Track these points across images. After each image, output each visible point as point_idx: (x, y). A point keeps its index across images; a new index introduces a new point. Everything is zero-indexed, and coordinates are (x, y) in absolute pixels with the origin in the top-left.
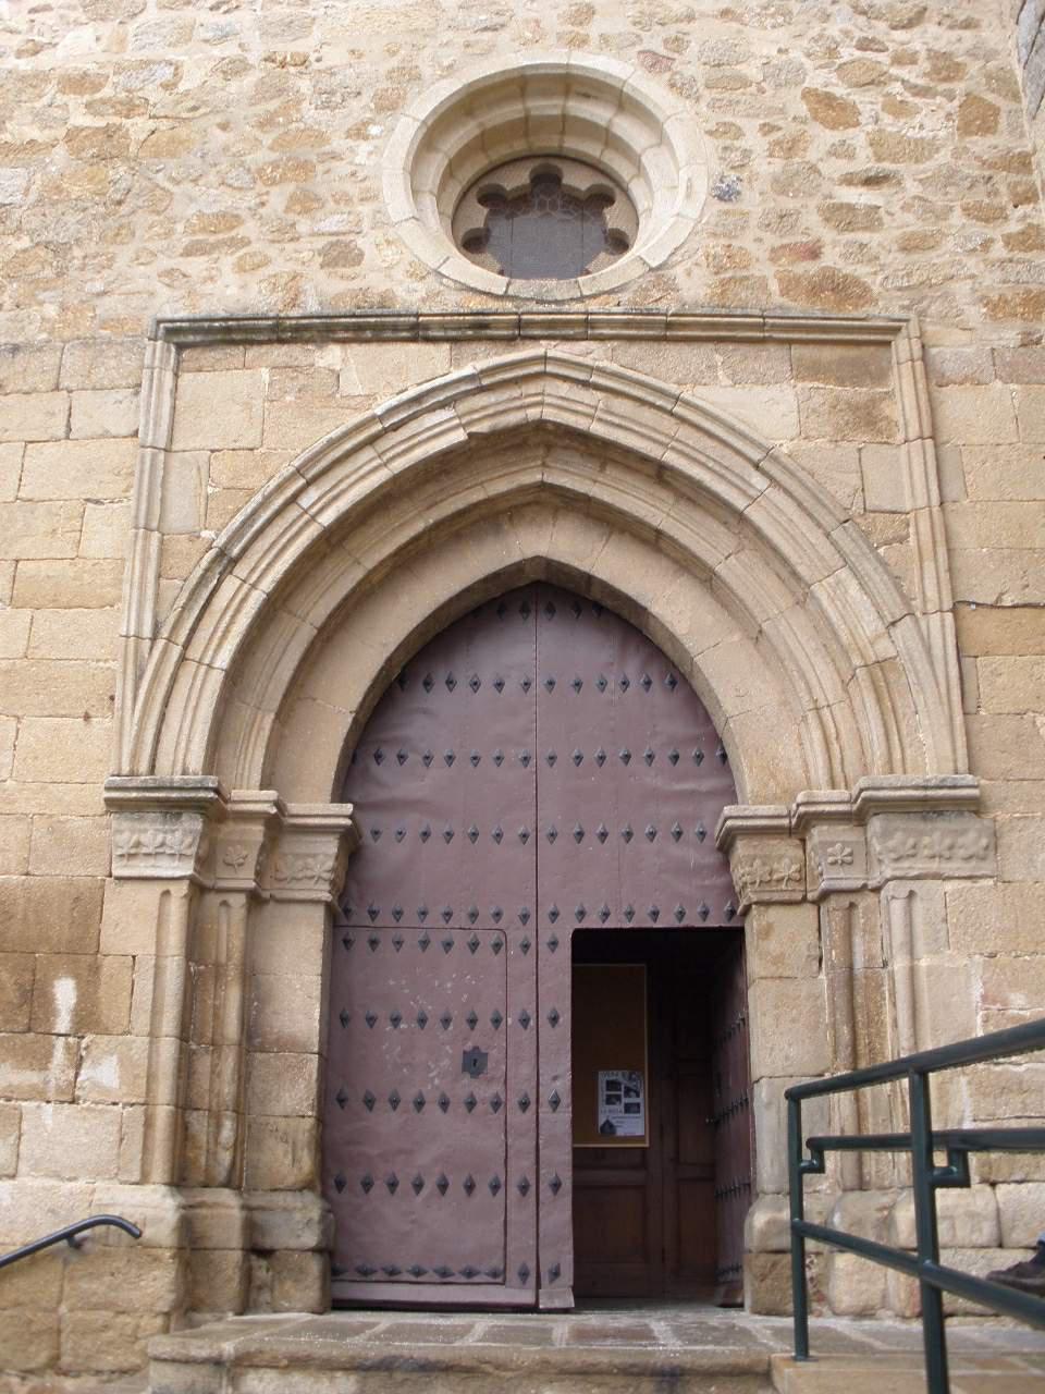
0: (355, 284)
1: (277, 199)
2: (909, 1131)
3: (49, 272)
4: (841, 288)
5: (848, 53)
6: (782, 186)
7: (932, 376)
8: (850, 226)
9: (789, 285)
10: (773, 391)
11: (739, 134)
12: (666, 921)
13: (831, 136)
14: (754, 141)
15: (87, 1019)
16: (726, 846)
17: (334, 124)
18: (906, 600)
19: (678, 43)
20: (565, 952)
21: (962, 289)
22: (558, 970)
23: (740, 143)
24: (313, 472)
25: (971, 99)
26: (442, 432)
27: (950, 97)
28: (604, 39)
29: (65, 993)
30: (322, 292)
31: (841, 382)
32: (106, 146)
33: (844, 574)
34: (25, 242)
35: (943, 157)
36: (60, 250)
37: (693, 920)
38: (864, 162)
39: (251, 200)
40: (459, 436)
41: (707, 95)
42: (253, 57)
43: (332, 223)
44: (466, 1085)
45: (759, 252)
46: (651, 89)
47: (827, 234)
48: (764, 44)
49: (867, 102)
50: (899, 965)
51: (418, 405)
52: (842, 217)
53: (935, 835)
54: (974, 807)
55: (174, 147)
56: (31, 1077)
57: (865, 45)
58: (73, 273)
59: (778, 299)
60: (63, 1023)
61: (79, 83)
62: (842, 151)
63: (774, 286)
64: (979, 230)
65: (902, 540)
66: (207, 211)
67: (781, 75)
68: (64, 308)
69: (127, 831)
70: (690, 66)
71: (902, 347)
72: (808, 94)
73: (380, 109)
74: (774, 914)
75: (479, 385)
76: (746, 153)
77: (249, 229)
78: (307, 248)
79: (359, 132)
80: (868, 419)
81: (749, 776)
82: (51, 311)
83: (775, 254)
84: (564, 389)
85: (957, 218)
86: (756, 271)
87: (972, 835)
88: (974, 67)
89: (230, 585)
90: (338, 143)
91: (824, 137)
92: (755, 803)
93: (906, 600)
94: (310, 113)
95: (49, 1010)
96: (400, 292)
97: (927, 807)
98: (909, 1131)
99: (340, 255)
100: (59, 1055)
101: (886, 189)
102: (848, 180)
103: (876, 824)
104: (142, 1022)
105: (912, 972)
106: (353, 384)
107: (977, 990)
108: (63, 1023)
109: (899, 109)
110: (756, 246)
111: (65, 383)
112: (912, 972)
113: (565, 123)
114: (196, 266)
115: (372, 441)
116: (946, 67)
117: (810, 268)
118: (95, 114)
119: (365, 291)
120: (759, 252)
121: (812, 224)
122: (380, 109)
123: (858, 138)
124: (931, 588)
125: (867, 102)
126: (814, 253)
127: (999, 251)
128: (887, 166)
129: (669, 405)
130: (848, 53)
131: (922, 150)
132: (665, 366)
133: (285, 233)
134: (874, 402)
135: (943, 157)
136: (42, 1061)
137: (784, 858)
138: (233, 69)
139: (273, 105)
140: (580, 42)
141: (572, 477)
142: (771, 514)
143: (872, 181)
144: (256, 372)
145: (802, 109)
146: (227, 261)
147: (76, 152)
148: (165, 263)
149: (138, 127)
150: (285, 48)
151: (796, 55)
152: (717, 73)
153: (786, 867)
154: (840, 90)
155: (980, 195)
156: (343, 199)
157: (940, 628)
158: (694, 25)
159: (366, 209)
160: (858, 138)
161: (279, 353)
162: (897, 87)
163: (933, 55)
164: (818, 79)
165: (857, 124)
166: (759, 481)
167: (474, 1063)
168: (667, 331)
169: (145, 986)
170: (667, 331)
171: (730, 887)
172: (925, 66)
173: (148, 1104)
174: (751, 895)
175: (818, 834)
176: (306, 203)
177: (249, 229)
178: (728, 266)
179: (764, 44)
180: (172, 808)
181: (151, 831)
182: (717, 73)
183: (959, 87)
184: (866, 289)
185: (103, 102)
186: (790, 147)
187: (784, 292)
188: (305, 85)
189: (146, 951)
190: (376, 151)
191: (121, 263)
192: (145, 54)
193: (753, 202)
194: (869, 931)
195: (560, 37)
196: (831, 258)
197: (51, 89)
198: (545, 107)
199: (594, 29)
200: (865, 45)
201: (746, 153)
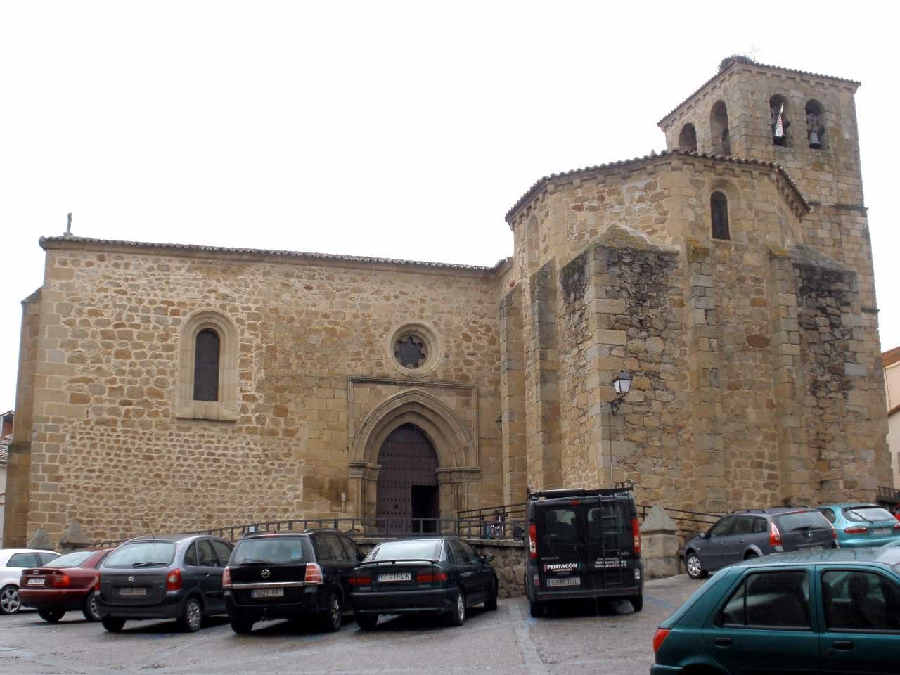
0: (382, 371)
1: (367, 349)
3: (325, 362)
4: (465, 378)
5: (471, 324)
6: (457, 355)
7: (479, 396)
8: (468, 365)
9: (457, 376)
10: (451, 398)
11: (450, 343)
12: (426, 484)
15: (347, 500)
16: (436, 474)
17: (377, 333)
18: (471, 437)
19: (440, 319)
20: (411, 489)
21: (486, 379)
22: (409, 491)
23: (450, 345)
24: (378, 410)
25: (492, 336)
26: (399, 403)
27: (488, 335)
29: (343, 495)
30: (377, 372)
31: (464, 396)
32: (332, 332)
33: (461, 432)
34: (320, 354)
35: (485, 350)
36: (327, 357)
37: (430, 484)
38: (472, 350)
39: (362, 350)
40: (401, 404)
41: (445, 332)
42: (360, 314)
43: (377, 357)
44: (394, 511)
46: (435, 330)
48: (457, 320)
50: (466, 495)
52: (467, 363)
53: (472, 476)
54: (478, 472)
55: (346, 335)
56: (339, 509)
57: (474, 322)
58: (330, 362)
59: (455, 380)
60: (343, 500)
61: (326, 316)
62: (468, 347)
63: (454, 377)
64: (490, 366)
65: (471, 426)
67: (459, 328)
68: (329, 370)
69: (352, 471)
70: (442, 326)
71: (475, 391)
72: (463, 333)
73: (385, 331)
74: (446, 485)
75: (405, 395)
76: (451, 347)
77: (362, 356)
78: (374, 362)
80: (467, 404)
81: (442, 462)
82: (327, 370)
83: (455, 370)
84: (418, 396)
85: (486, 364)
86: (451, 374)
87: (478, 476)
88: (493, 329)
89: (366, 429)
90: (378, 338)
91: (465, 344)
92: (442, 468)
93: (471, 437)
95: (341, 498)
96: (390, 373)
97: (472, 472)
99: (379, 365)
100: (343, 505)
101: (474, 357)
102: (468, 354)
103: (463, 473)
104: (356, 500)
105: (468, 496)
106: (384, 393)
107: (477, 499)
108: (343, 500)
109: (479, 338)
111: (333, 387)
112: (468, 496)
113: (417, 331)
114: (353, 363)
115: (387, 404)
116: (488, 329)
117: (460, 373)
118: (330, 324)
119: (384, 373)
120: (452, 369)
121: (462, 364)
122: (385, 331)
123: (471, 344)
124: (475, 435)
125: (473, 336)
126: (461, 370)
127: (493, 371)
128: (476, 351)
129: (435, 400)
130: (471, 324)
131: (483, 347)
132: (434, 393)
133: (368, 358)
134: (469, 400)
135: (485, 350)
136: (340, 506)
137: (448, 477)
138: (356, 316)
140: (421, 317)
141: (417, 409)
142: (451, 421)
143: (473, 354)
144: (365, 390)
145: (461, 337)
146: (359, 363)
147: (327, 333)
148: (347, 362)
149: (338, 329)
150: (366, 313)
151: (461, 324)
153: (448, 478)
154: (469, 333)
155: (491, 359)
156: (379, 352)
157: (476, 442)
158: (444, 315)
159: (383, 354)
160: (471, 344)
161: (371, 385)
162: (479, 333)
163: (487, 326)
164: (465, 330)
165: (471, 341)
166: (449, 415)
167: (396, 507)
168: (433, 385)
169: (356, 495)
170: (433, 385)
171: (437, 479)
172: (484, 328)
173: (358, 513)
174: (443, 482)
175: (453, 474)
176: (372, 351)
177: (362, 356)
178: (446, 371)
179: (457, 320)
180: (359, 467)
181: (356, 471)
183: (490, 334)
184: (469, 378)
185: (331, 321)
187: (456, 378)
189: (356, 490)
191: (339, 361)
192: (337, 310)
193: (451, 359)
194: (461, 489)
195: (418, 316)
196: (464, 371)
198: (414, 328)
200: (474, 322)
201: (451, 347)
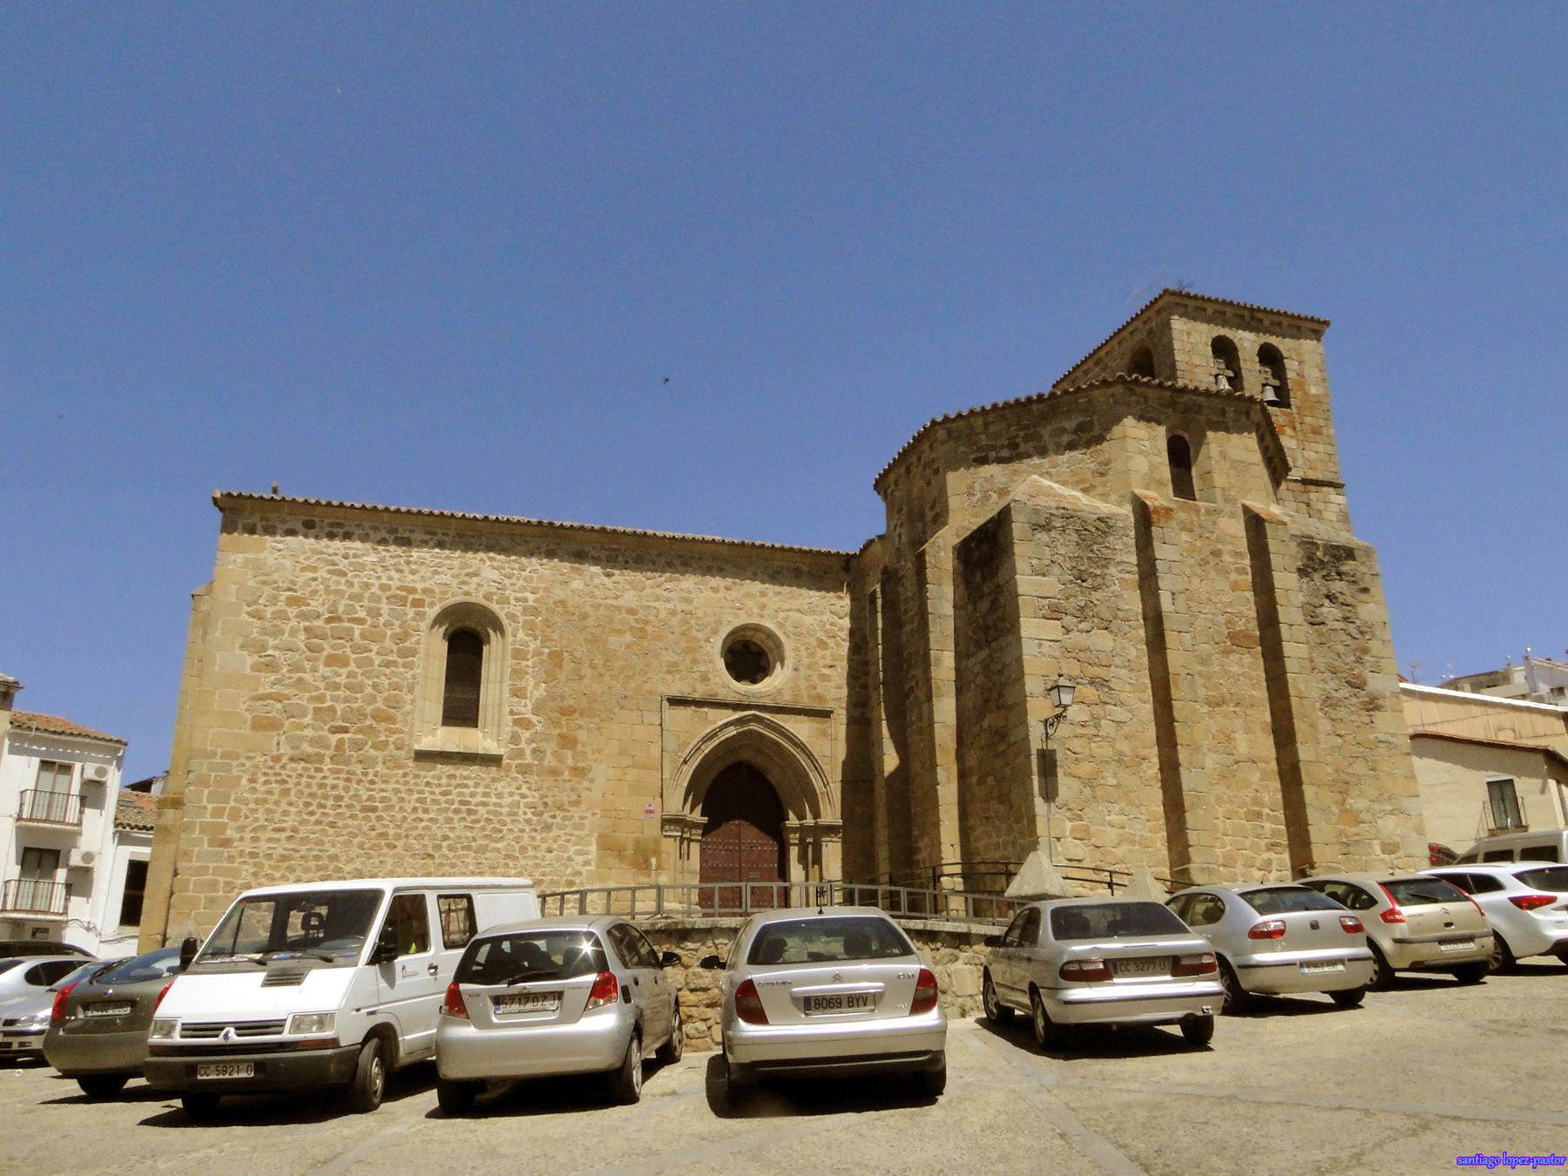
2: (1129, 421)
4: (820, 698)
5: (828, 627)
9: (809, 696)
13: (822, 653)
14: (803, 653)
15: (659, 867)
28: (768, 615)
29: (654, 861)
38: (829, 662)
42: (679, 610)
45: (803, 687)
47: (818, 682)
49: (831, 642)
51: (726, 725)
57: (832, 624)
61: (632, 611)
66: (1001, 1003)
72: (818, 639)
78: (697, 675)
79: (707, 640)
83: (806, 687)
94: (695, 633)
98: (1129, 421)
99: (704, 678)
102: (824, 667)
110: (803, 684)
114: (669, 677)
117: (815, 692)
120: (803, 687)
121: (815, 678)
128: (834, 663)
139: (685, 628)
146: (677, 677)
149: (650, 629)
152: (796, 630)
160: (828, 653)
164: (820, 634)
176: (695, 661)
182: (796, 630)
186: (812, 655)
188: (693, 622)
190: (712, 647)
196: (819, 690)
197: (624, 612)
199: (766, 612)
